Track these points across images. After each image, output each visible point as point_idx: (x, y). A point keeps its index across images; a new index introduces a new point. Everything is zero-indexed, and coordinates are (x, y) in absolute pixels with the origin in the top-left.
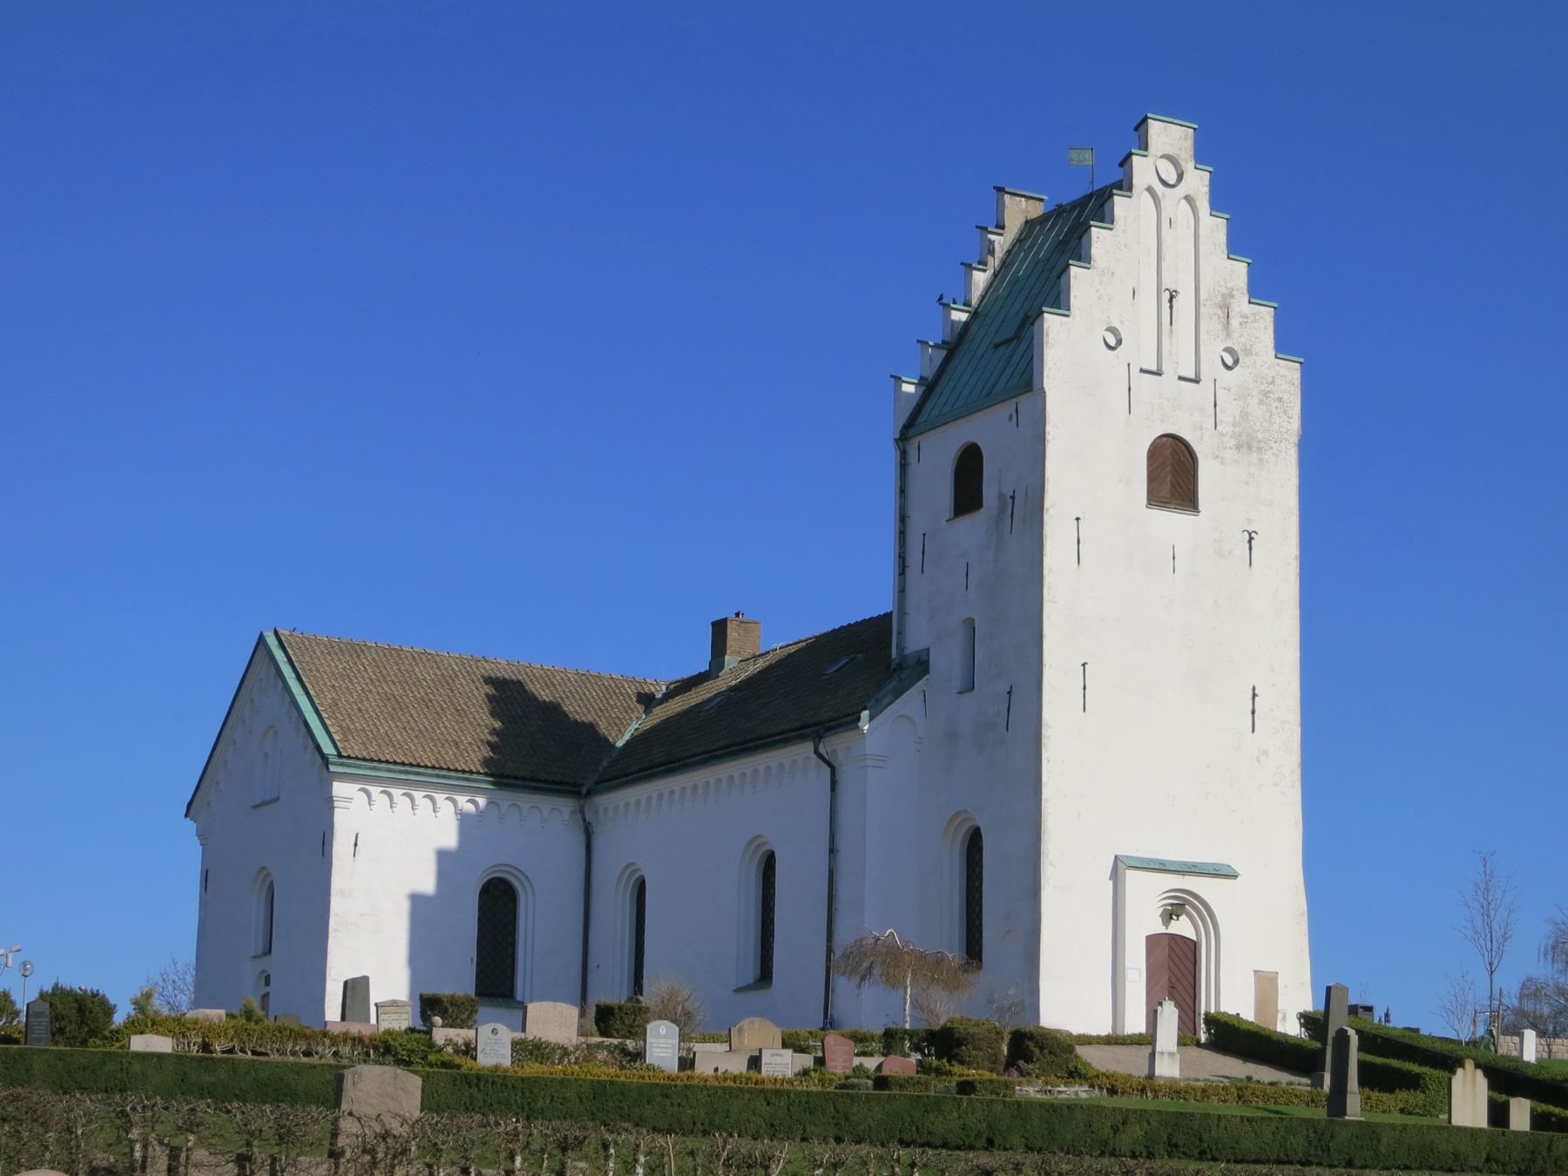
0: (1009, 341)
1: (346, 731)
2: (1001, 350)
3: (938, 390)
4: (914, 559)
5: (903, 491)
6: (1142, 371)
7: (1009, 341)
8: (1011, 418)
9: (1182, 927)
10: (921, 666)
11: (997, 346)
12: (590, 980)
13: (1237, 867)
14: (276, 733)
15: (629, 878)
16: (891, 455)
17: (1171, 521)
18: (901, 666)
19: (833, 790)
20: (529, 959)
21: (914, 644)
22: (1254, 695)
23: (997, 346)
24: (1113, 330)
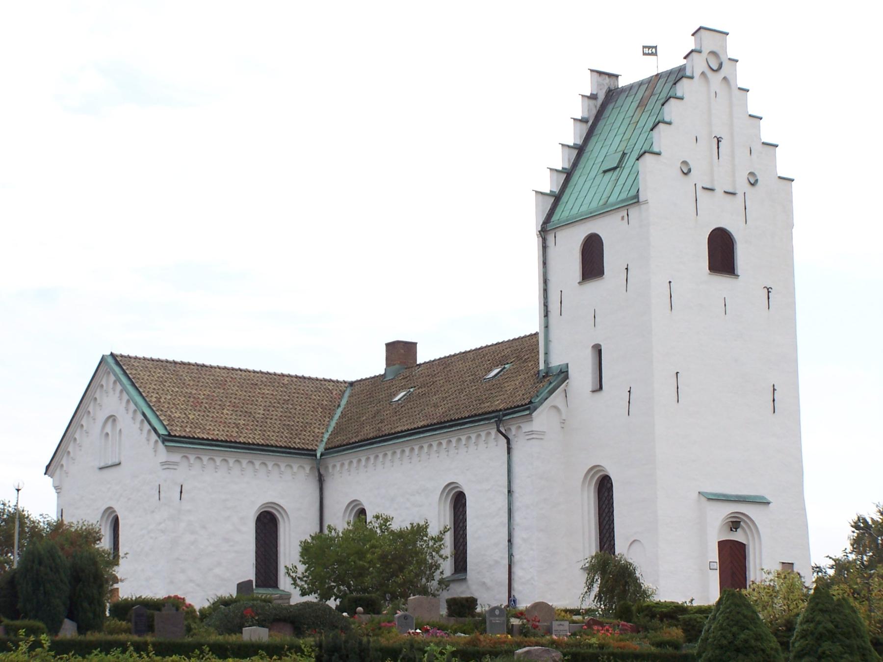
0: (615, 169)
1: (170, 418)
2: (609, 174)
3: (564, 198)
4: (554, 307)
5: (545, 263)
6: (703, 188)
7: (615, 169)
8: (623, 218)
9: (738, 536)
10: (563, 374)
11: (605, 172)
12: (507, 576)
13: (770, 500)
14: (114, 420)
15: (352, 509)
16: (534, 242)
17: (722, 282)
18: (548, 373)
19: (509, 453)
20: (758, 561)
21: (556, 361)
22: (774, 390)
23: (605, 172)
24: (685, 163)
